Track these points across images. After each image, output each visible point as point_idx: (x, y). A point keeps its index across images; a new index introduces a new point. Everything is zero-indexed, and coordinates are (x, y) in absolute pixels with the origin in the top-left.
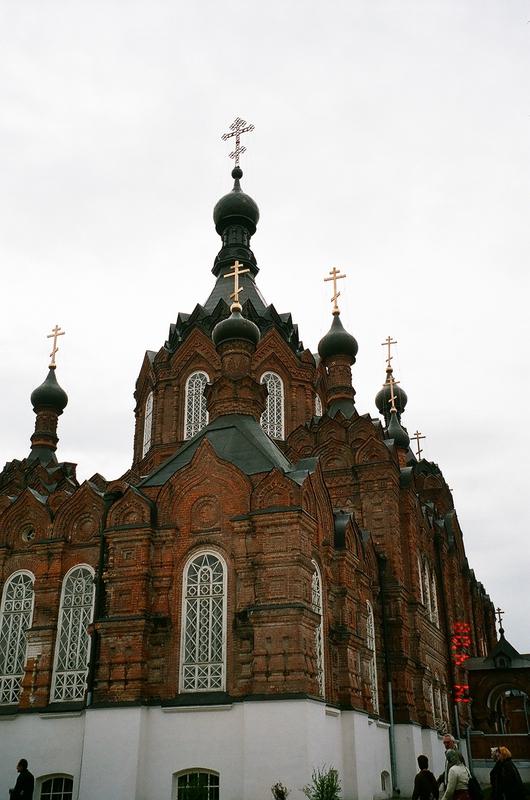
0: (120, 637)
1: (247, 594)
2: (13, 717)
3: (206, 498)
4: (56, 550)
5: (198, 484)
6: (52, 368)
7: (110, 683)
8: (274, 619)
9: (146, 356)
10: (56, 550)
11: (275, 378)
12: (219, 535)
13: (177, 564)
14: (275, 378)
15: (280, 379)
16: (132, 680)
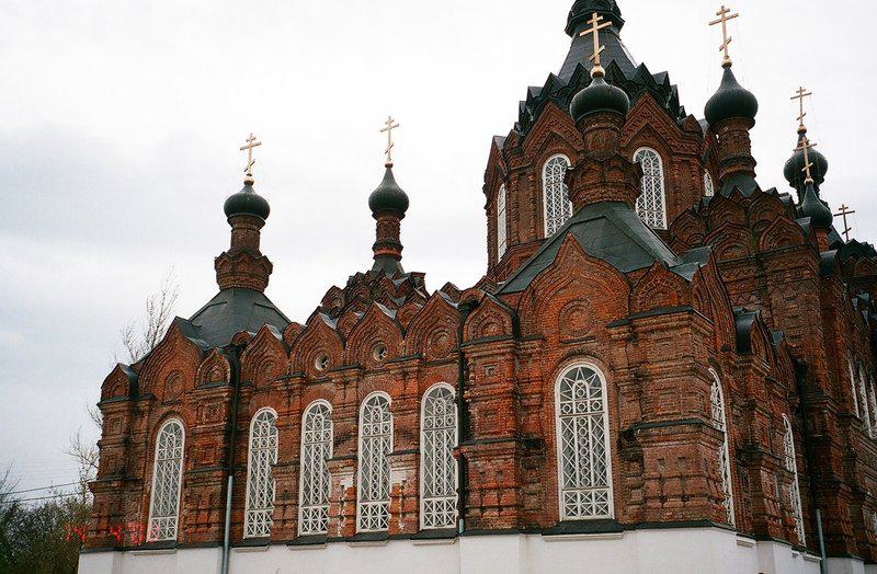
0: (490, 461)
1: (632, 411)
2: (323, 546)
3: (576, 303)
4: (411, 369)
5: (564, 288)
6: (389, 166)
7: (483, 509)
8: (666, 438)
9: (494, 143)
10: (411, 369)
11: (652, 154)
12: (593, 345)
13: (546, 379)
14: (652, 154)
15: (658, 156)
16: (507, 507)
